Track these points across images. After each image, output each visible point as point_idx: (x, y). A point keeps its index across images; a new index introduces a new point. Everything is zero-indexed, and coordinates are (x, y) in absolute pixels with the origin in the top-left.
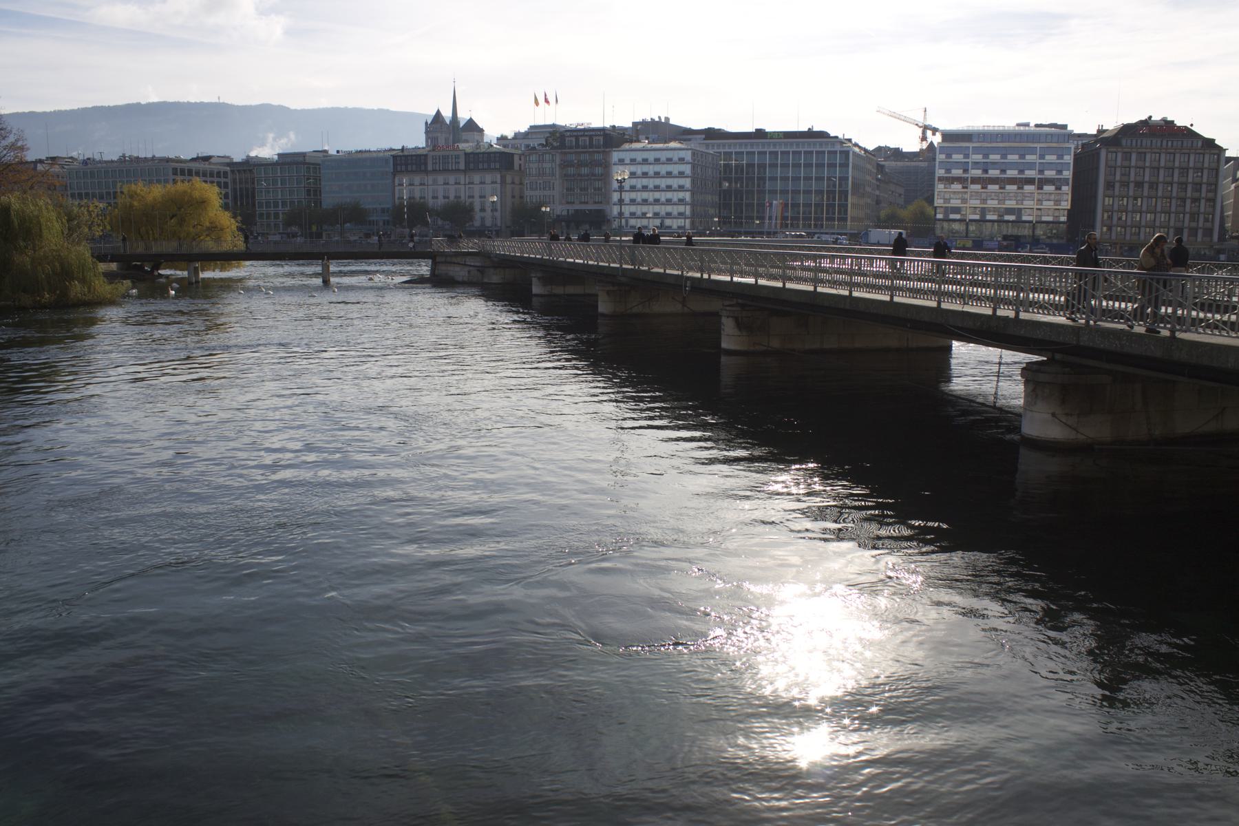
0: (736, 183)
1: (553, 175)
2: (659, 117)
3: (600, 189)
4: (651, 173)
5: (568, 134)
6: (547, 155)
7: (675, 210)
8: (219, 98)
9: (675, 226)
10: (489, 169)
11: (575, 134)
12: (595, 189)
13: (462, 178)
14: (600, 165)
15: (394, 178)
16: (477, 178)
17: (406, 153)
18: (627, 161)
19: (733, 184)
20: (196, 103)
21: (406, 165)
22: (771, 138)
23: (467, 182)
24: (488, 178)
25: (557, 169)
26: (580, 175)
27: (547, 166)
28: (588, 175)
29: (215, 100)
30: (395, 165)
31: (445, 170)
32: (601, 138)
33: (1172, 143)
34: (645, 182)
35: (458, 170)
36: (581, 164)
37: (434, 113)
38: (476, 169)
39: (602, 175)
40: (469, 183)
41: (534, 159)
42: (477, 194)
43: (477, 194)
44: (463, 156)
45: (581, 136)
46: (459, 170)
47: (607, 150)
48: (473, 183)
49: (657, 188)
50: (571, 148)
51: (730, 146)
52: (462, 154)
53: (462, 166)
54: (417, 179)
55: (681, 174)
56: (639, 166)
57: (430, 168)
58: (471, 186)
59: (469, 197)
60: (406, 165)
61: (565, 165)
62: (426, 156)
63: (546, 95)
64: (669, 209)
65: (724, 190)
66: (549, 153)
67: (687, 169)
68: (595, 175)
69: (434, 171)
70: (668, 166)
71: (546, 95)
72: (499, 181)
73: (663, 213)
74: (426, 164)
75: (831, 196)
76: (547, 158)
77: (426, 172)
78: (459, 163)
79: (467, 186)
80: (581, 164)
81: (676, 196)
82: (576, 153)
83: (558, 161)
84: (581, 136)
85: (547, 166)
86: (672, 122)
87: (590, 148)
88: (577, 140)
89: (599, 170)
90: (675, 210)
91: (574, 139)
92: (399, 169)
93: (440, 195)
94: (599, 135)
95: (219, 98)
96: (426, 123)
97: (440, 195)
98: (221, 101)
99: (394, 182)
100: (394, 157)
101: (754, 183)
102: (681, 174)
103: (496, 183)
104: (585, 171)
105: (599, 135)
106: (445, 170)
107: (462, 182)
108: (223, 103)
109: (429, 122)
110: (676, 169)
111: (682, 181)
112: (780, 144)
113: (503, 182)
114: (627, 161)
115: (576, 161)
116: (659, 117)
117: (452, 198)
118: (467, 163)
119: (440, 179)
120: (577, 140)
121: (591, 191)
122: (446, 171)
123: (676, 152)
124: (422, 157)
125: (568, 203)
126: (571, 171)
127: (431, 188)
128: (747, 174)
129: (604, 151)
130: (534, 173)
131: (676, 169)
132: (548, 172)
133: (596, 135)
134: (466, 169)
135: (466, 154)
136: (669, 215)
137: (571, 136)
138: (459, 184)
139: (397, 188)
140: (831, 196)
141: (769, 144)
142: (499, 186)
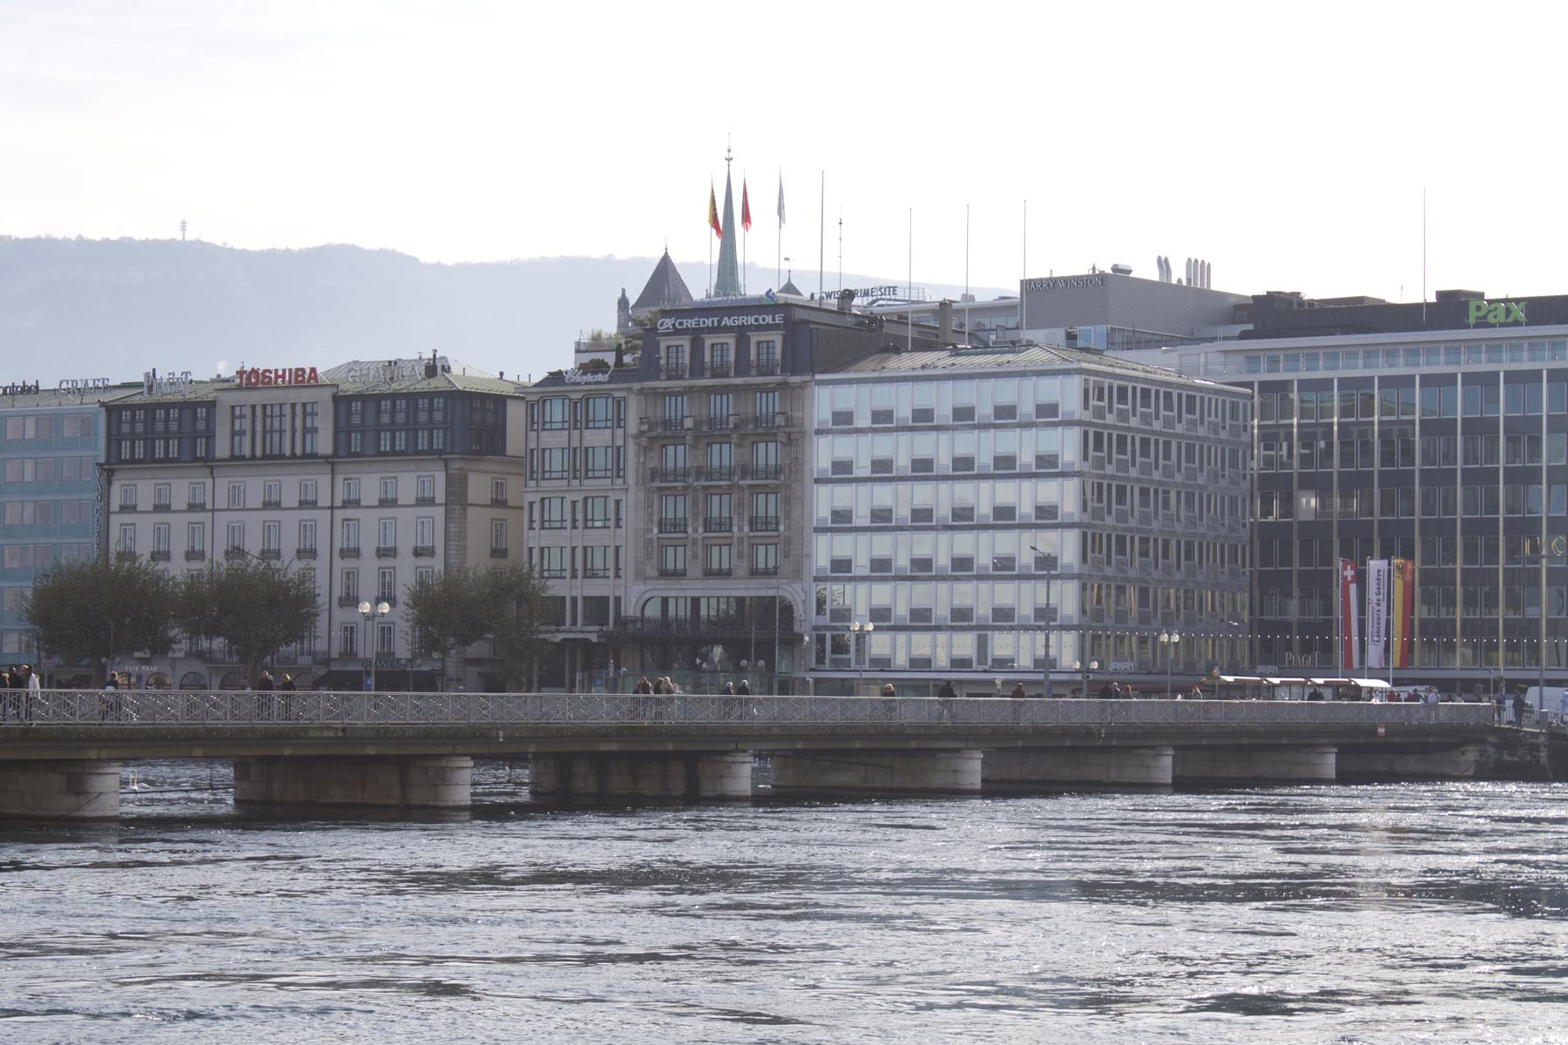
0: (1346, 497)
1: (619, 472)
2: (1163, 264)
3: (770, 524)
4: (944, 462)
5: (669, 322)
6: (600, 403)
7: (1024, 598)
8: (183, 228)
9: (901, 660)
10: (412, 454)
11: (690, 323)
12: (753, 523)
13: (321, 484)
14: (769, 435)
15: (110, 483)
16: (370, 484)
17: (156, 397)
18: (863, 420)
19: (1337, 502)
20: (106, 243)
21: (412, 428)
22: (1482, 323)
23: (338, 503)
24: (407, 483)
25: (632, 448)
26: (746, 471)
27: (597, 438)
28: (731, 473)
29: (166, 231)
30: (113, 440)
31: (273, 457)
32: (777, 338)
33: (1206, 357)
34: (923, 494)
35: (311, 457)
36: (710, 432)
37: (662, 255)
38: (375, 455)
39: (778, 471)
40: (347, 504)
41: (558, 417)
42: (368, 544)
43: (368, 544)
44: (330, 406)
45: (712, 330)
46: (314, 456)
47: (796, 379)
48: (355, 503)
49: (963, 518)
50: (675, 375)
51: (1273, 364)
52: (326, 395)
53: (324, 444)
54: (180, 489)
55: (1047, 466)
56: (904, 438)
57: (222, 449)
58: (351, 513)
59: (345, 554)
60: (412, 428)
61: (660, 434)
62: (211, 405)
63: (713, 192)
64: (1005, 594)
65: (1304, 525)
66: (606, 395)
67: (1067, 445)
68: (755, 473)
69: (236, 459)
70: (1002, 435)
71: (713, 192)
72: (440, 497)
73: (983, 612)
74: (210, 436)
75: (1481, 542)
76: (601, 415)
77: (209, 462)
78: (314, 430)
79: (340, 514)
80: (710, 432)
81: (1021, 546)
82: (690, 391)
83: (633, 425)
84: (712, 330)
85: (597, 438)
86: (1219, 283)
87: (738, 374)
88: (697, 346)
89: (767, 454)
90: (1024, 598)
91: (685, 342)
92: (125, 453)
93: (179, 547)
94: (768, 327)
95: (183, 228)
96: (623, 302)
97: (179, 547)
98: (190, 236)
99: (106, 496)
100: (112, 410)
101: (1410, 494)
102: (1047, 466)
103: (430, 502)
104: (723, 455)
105: (768, 327)
106: (273, 457)
107: (324, 500)
108: (198, 242)
109: (633, 299)
110: (1025, 446)
111: (1047, 491)
112: (1515, 345)
113: (457, 497)
114: (863, 420)
115: (689, 423)
116: (1163, 264)
117: (217, 553)
118: (341, 431)
119: (254, 486)
120: (697, 346)
121: (741, 529)
122: (273, 458)
123: (1029, 383)
124: (201, 412)
125: (664, 574)
126: (676, 457)
127: (222, 519)
128: (1426, 458)
129: (783, 386)
130: (557, 466)
131: (1025, 446)
132: (557, 466)
133: (759, 328)
134: (335, 455)
135: (337, 399)
136: (1004, 617)
137: (676, 332)
138: (313, 505)
139: (116, 520)
140: (1481, 542)
141: (1473, 346)
142: (439, 513)
